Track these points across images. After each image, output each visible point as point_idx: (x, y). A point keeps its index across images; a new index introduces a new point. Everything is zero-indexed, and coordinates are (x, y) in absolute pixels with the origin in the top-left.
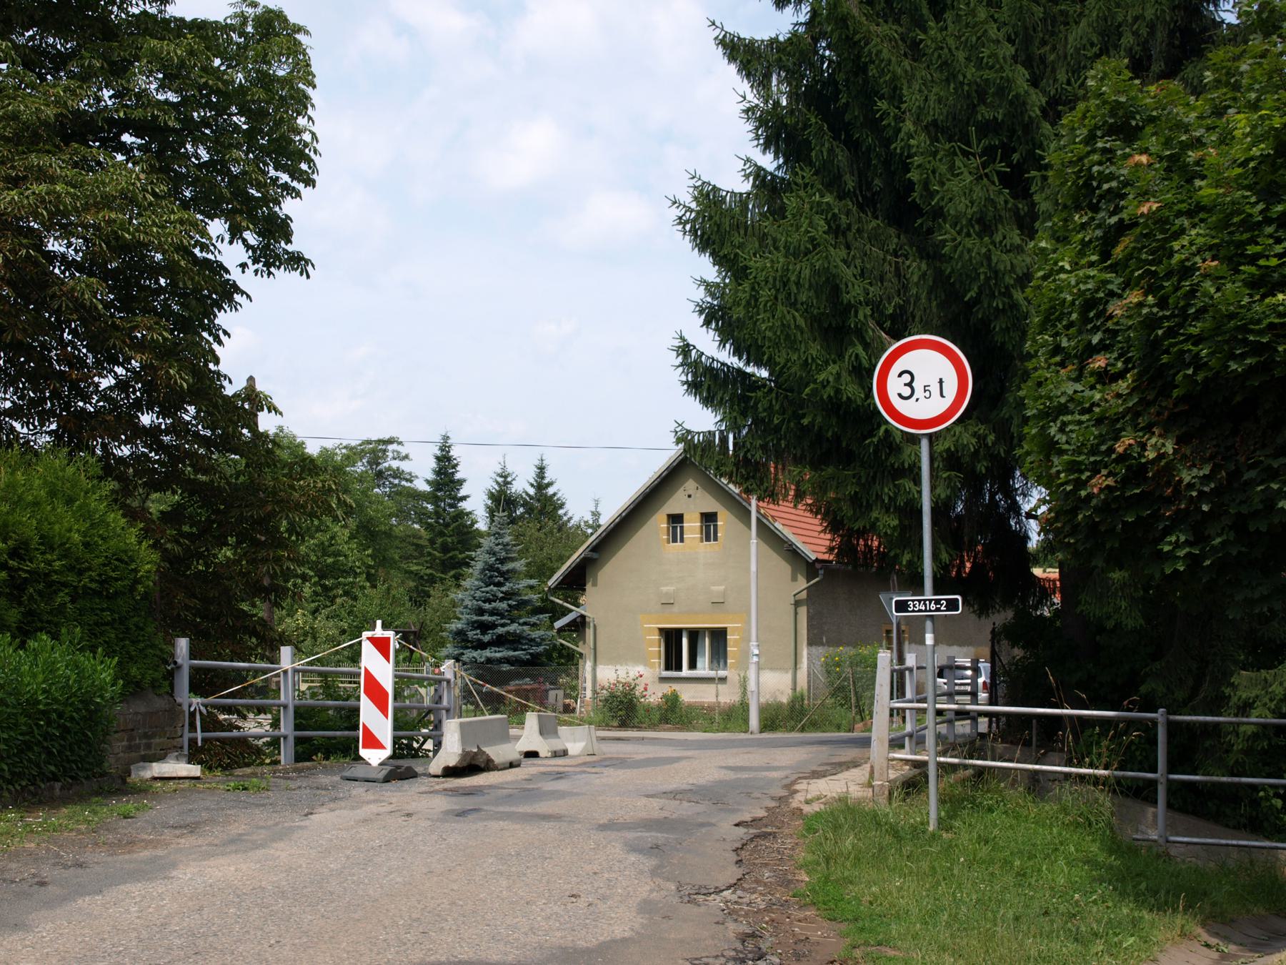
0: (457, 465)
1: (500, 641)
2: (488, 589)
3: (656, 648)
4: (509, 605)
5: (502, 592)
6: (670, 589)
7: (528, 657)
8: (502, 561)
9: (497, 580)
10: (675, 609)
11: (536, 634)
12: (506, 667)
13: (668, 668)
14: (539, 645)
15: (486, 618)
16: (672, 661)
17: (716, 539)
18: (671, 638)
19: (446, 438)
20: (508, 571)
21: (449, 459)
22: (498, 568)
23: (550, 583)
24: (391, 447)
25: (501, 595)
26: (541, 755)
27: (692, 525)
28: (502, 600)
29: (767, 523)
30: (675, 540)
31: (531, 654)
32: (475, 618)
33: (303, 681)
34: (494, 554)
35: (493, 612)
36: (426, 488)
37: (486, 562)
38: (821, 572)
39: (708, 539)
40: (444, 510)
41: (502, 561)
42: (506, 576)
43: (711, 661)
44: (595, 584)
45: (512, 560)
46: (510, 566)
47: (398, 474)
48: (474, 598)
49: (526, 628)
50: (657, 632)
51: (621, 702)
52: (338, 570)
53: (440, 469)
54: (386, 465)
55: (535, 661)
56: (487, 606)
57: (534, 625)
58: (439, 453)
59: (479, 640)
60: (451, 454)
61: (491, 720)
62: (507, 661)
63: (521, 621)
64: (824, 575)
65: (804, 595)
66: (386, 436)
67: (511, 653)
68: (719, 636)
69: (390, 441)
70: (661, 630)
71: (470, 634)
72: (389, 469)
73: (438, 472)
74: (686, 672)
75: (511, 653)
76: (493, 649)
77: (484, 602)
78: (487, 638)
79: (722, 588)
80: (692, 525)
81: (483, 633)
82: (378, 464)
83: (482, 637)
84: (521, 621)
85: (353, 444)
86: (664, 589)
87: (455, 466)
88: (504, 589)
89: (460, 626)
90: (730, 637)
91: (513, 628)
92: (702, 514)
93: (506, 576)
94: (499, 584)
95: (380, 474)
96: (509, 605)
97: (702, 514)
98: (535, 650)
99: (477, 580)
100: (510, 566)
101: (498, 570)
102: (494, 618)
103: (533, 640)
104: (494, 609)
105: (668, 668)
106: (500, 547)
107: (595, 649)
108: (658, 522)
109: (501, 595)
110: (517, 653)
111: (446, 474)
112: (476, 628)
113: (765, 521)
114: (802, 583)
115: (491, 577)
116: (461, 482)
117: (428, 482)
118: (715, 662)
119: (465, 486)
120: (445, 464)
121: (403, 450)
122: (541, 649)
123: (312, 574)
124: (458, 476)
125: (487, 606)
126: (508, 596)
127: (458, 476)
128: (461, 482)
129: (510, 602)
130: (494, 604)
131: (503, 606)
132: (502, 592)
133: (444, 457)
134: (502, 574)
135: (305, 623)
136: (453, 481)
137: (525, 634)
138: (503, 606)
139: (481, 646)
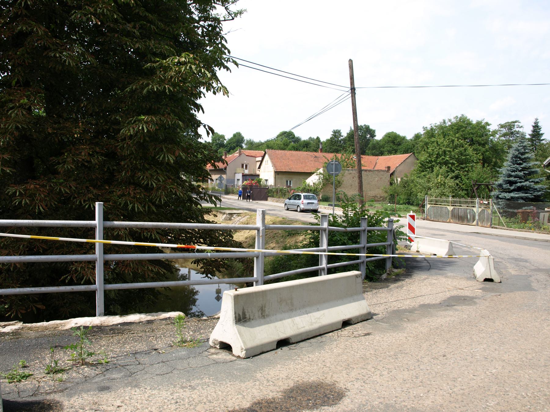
0: (541, 128)
1: (519, 189)
2: (514, 166)
4: (524, 173)
5: (521, 168)
7: (533, 197)
8: (523, 154)
9: (519, 162)
11: (537, 186)
12: (521, 201)
13: (96, 316)
14: (540, 191)
15: (512, 179)
19: (537, 119)
20: (525, 158)
21: (538, 127)
22: (520, 157)
23: (544, 163)
24: (516, 124)
25: (520, 169)
28: (520, 171)
31: (534, 196)
32: (507, 179)
33: (428, 204)
34: (518, 150)
35: (516, 177)
36: (529, 137)
37: (513, 154)
40: (535, 144)
41: (523, 154)
42: (525, 160)
45: (527, 153)
46: (526, 155)
47: (518, 132)
49: (532, 183)
52: (466, 161)
53: (534, 130)
54: (514, 130)
55: (537, 199)
56: (513, 174)
57: (537, 182)
58: (534, 125)
60: (539, 125)
61: (263, 293)
62: (522, 198)
63: (530, 180)
66: (514, 120)
67: (523, 195)
69: (516, 122)
71: (504, 186)
72: (515, 131)
73: (533, 131)
75: (523, 195)
78: (512, 188)
81: (511, 186)
82: (512, 130)
83: (509, 187)
84: (530, 180)
85: (502, 124)
87: (540, 129)
91: (527, 183)
93: (525, 160)
94: (520, 164)
95: (512, 133)
96: (524, 173)
98: (536, 193)
99: (510, 162)
100: (526, 155)
101: (519, 158)
102: (516, 179)
103: (536, 189)
104: (516, 175)
106: (521, 147)
110: (526, 195)
111: (536, 132)
112: (507, 183)
115: (516, 161)
116: (542, 134)
117: (529, 135)
119: (544, 135)
120: (536, 128)
121: (520, 125)
122: (539, 193)
123: (456, 163)
124: (541, 132)
125: (513, 174)
126: (524, 169)
127: (541, 132)
128: (542, 134)
129: (525, 172)
130: (516, 173)
131: (521, 174)
132: (521, 168)
133: (536, 126)
134: (521, 159)
135: (441, 180)
136: (539, 134)
137: (532, 186)
138: (521, 174)
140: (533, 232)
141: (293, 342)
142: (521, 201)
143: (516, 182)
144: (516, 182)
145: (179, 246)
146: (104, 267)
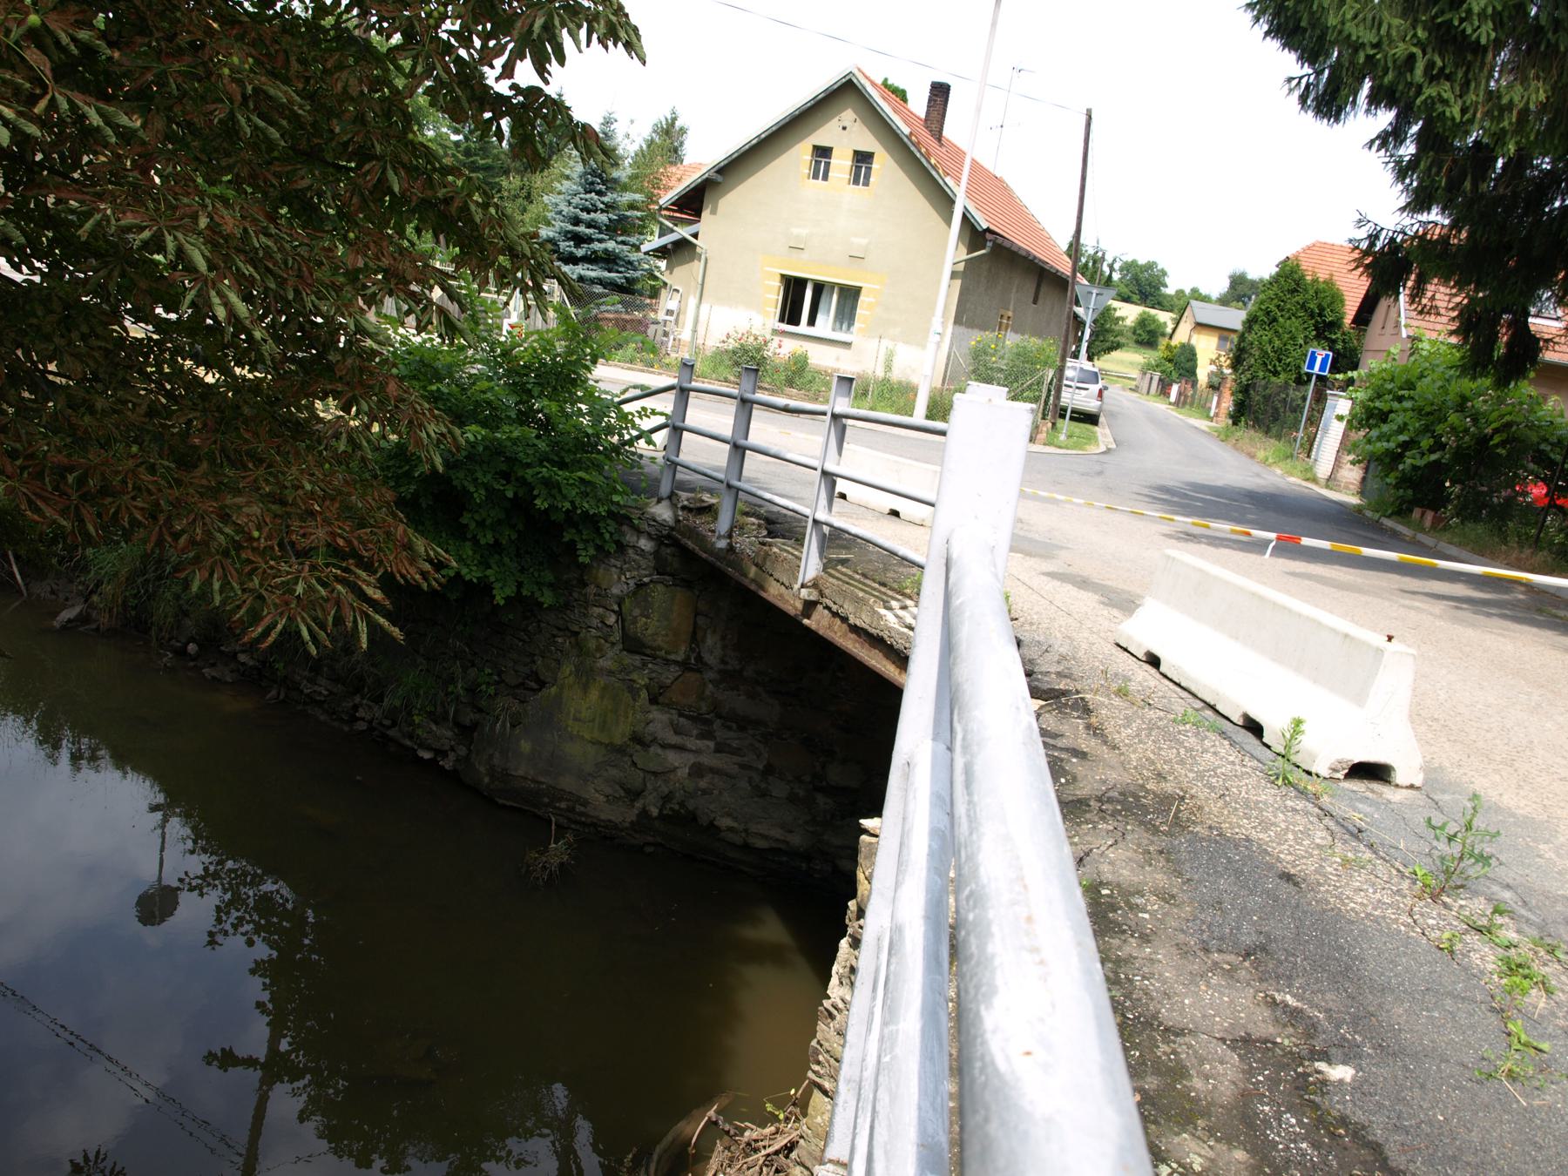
1: (592, 259)
2: (588, 196)
3: (774, 296)
6: (803, 232)
10: (804, 255)
13: (782, 320)
14: (635, 269)
15: (582, 229)
16: (790, 313)
17: (866, 183)
18: (793, 287)
25: (602, 206)
26: (1400, 777)
27: (841, 163)
28: (603, 211)
29: (936, 176)
30: (815, 176)
31: (626, 278)
32: (571, 227)
38: (989, 244)
39: (856, 182)
43: (835, 321)
44: (714, 212)
48: (570, 203)
50: (778, 278)
51: (753, 358)
56: (584, 216)
59: (571, 253)
62: (600, 282)
64: (993, 249)
65: (961, 267)
68: (850, 295)
70: (783, 276)
74: (803, 328)
75: (607, 274)
76: (586, 266)
77: (582, 210)
78: (580, 253)
79: (864, 241)
80: (841, 163)
81: (577, 246)
86: (795, 231)
88: (606, 199)
89: (551, 234)
90: (863, 298)
91: (611, 245)
92: (856, 153)
94: (599, 193)
97: (856, 153)
98: (631, 274)
103: (630, 263)
104: (593, 220)
105: (782, 320)
107: (703, 285)
108: (800, 153)
109: (602, 206)
110: (613, 275)
112: (569, 239)
113: (934, 173)
114: (963, 255)
115: (592, 183)
118: (838, 325)
125: (584, 216)
126: (610, 207)
130: (593, 215)
131: (602, 218)
139: (572, 260)
140: (660, 374)
141: (858, 1074)
142: (598, 289)
143: (589, 240)
144: (589, 240)
145: (270, 639)
146: (1122, 1035)
